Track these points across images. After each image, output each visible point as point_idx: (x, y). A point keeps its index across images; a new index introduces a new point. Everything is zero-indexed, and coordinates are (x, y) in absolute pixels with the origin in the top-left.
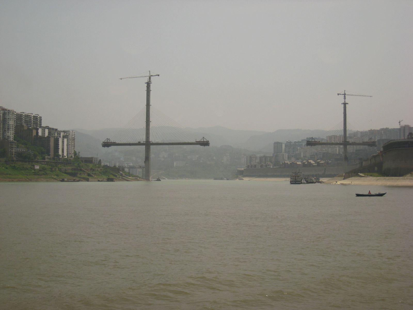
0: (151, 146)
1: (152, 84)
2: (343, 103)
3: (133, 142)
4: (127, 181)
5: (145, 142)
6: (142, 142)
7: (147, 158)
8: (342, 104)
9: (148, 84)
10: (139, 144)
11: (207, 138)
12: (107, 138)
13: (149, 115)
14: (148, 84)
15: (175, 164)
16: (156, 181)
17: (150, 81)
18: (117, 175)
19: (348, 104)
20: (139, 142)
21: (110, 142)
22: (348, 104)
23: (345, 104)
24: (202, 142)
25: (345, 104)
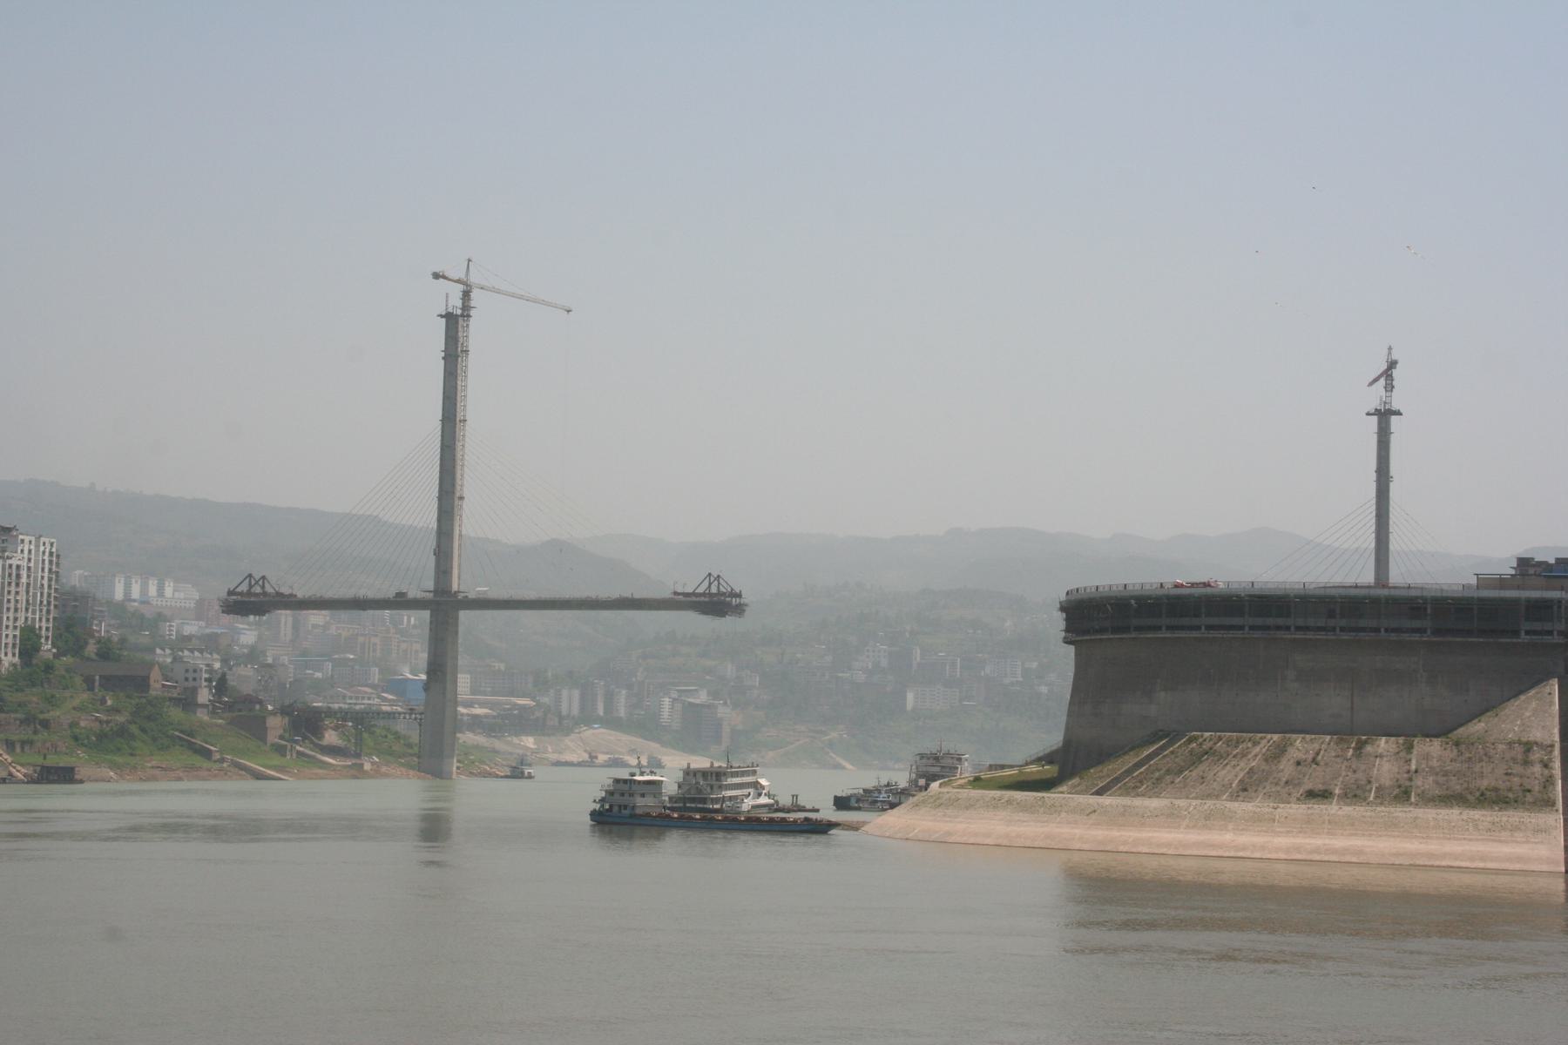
0: (464, 616)
1: (439, 313)
2: (1377, 412)
3: (380, 596)
4: (258, 779)
5: (430, 596)
6: (413, 593)
7: (439, 670)
8: (1368, 414)
9: (454, 322)
10: (400, 602)
11: (736, 580)
12: (250, 576)
13: (454, 467)
14: (454, 322)
15: (910, 696)
16: (507, 777)
17: (466, 307)
18: (210, 751)
19: (1398, 413)
20: (400, 595)
21: (722, 589)
22: (1398, 413)
23: (1384, 416)
24: (241, 594)
25: (1384, 416)
